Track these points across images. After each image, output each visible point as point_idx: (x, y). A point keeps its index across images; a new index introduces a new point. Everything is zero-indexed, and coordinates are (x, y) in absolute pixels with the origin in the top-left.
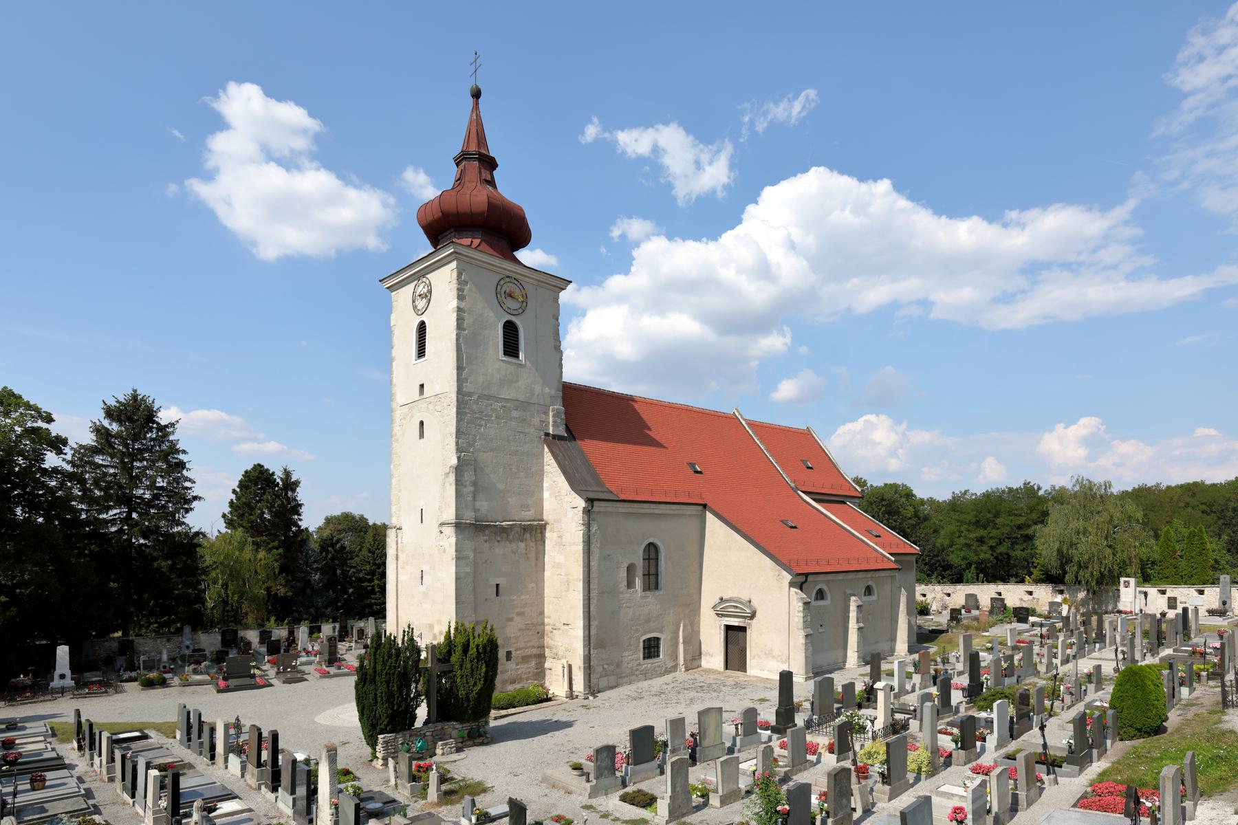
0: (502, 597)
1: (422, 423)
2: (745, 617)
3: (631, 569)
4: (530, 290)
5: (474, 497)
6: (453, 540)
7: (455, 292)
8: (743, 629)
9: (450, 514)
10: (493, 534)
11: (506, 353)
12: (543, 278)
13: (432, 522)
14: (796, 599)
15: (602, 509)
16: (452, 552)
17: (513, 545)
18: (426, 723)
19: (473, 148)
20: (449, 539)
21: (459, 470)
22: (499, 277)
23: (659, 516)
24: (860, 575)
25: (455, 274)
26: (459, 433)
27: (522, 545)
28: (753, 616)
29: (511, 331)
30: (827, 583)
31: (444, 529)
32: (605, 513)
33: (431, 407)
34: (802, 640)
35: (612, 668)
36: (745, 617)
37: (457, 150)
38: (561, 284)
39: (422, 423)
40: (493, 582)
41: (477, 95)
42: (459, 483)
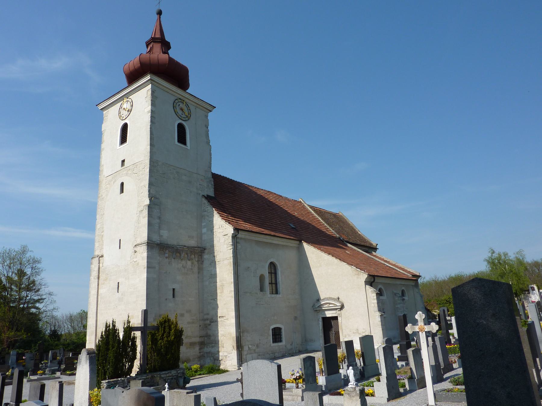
0: (177, 298)
1: (122, 184)
2: (336, 309)
3: (262, 278)
4: (192, 108)
5: (160, 227)
6: (145, 254)
7: (150, 102)
8: (336, 318)
9: (143, 236)
10: (172, 252)
11: (179, 141)
12: (200, 103)
13: (128, 247)
14: (372, 293)
15: (243, 236)
16: (144, 263)
17: (183, 262)
18: (138, 374)
19: (158, 36)
20: (143, 252)
21: (150, 207)
22: (173, 98)
23: (277, 246)
24: (398, 282)
25: (150, 92)
26: (151, 184)
27: (189, 263)
28: (342, 307)
29: (181, 130)
30: (384, 284)
31: (138, 249)
32: (245, 240)
33: (129, 172)
34: (379, 319)
35: (254, 348)
36: (336, 309)
37: (148, 38)
38: (210, 108)
39: (122, 184)
40: (171, 287)
41: (160, 13)
42: (150, 215)
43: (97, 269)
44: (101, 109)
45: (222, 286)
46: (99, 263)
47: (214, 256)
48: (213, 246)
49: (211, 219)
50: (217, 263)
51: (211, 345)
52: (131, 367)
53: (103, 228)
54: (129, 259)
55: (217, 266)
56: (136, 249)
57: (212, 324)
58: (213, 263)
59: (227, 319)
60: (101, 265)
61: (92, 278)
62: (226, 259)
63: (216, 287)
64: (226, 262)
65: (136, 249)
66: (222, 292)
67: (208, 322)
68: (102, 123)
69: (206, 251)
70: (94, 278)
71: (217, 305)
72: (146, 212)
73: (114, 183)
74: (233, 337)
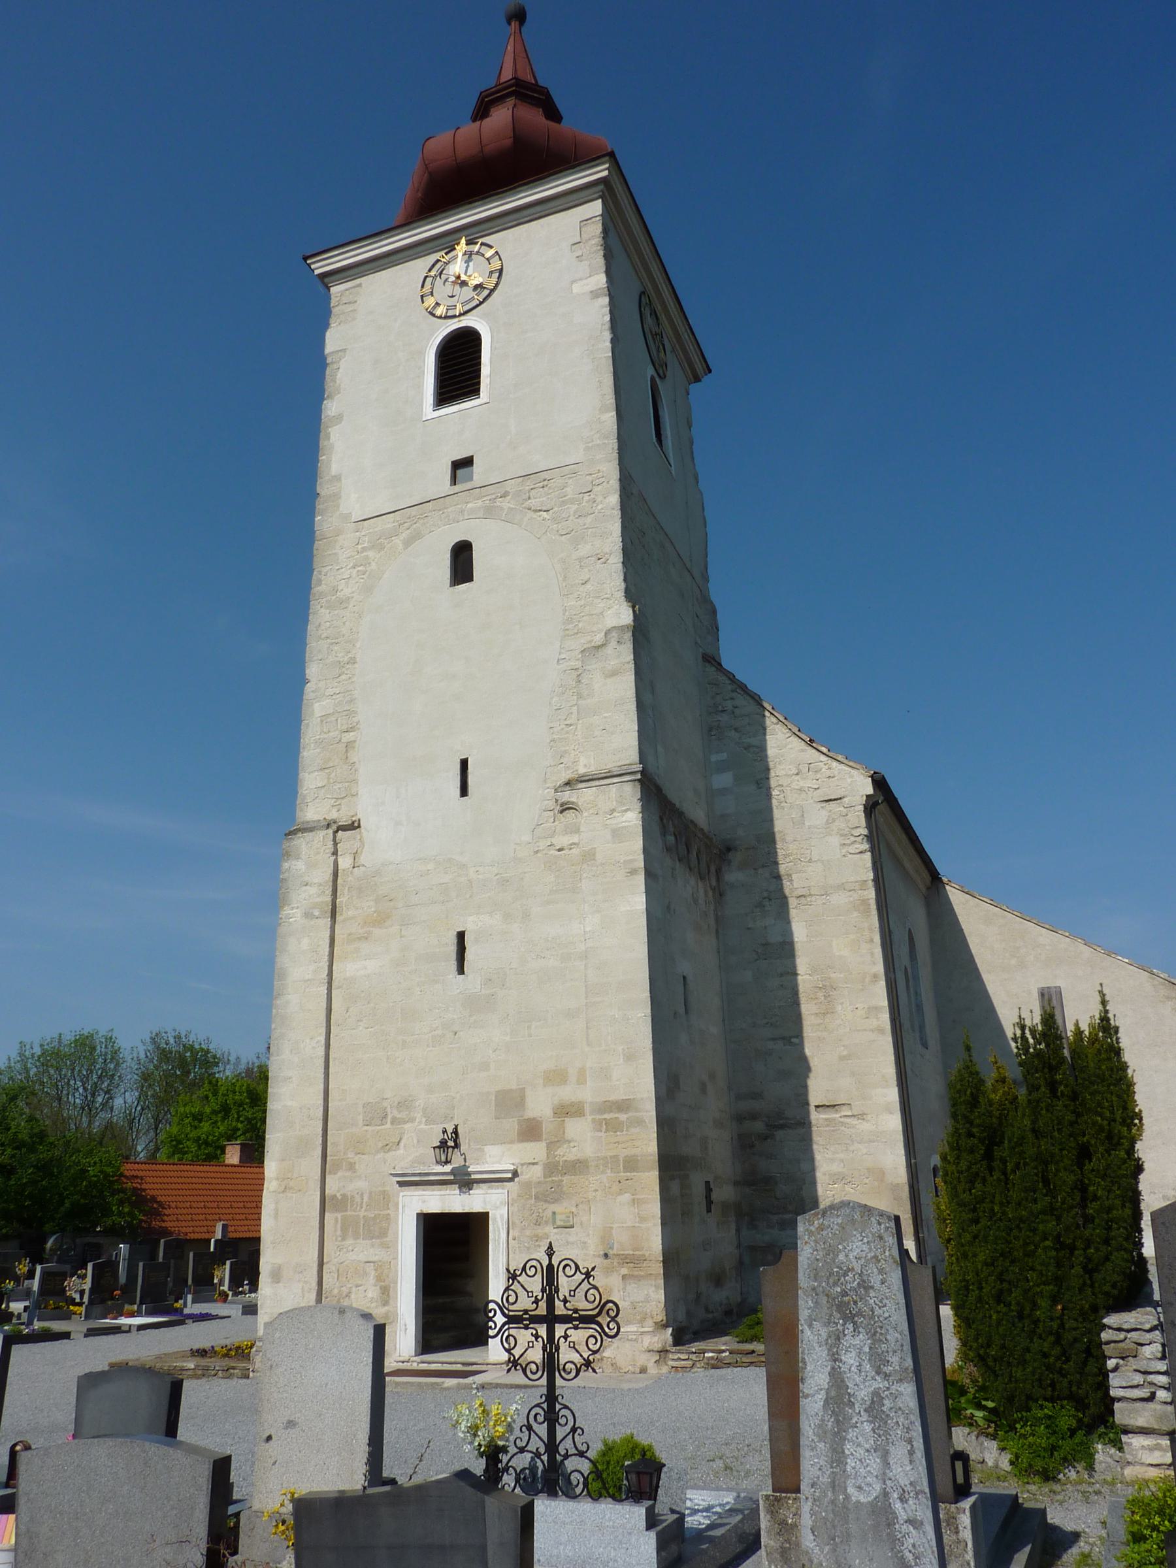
13: (516, 798)
25: (596, 229)
33: (506, 504)
38: (699, 368)
43: (323, 875)
44: (323, 276)
45: (828, 989)
46: (335, 853)
47: (778, 877)
48: (766, 841)
49: (754, 741)
50: (792, 902)
51: (775, 1218)
52: (132, 1315)
53: (351, 713)
54: (527, 838)
55: (793, 913)
56: (567, 796)
57: (780, 1134)
58: (774, 901)
59: (861, 1116)
60: (344, 862)
61: (293, 914)
62: (841, 887)
63: (796, 993)
64: (840, 899)
65: (567, 796)
66: (827, 1012)
67: (759, 1126)
68: (327, 326)
69: (736, 857)
70: (308, 915)
71: (804, 1059)
72: (622, 655)
73: (408, 543)
74: (895, 1188)
